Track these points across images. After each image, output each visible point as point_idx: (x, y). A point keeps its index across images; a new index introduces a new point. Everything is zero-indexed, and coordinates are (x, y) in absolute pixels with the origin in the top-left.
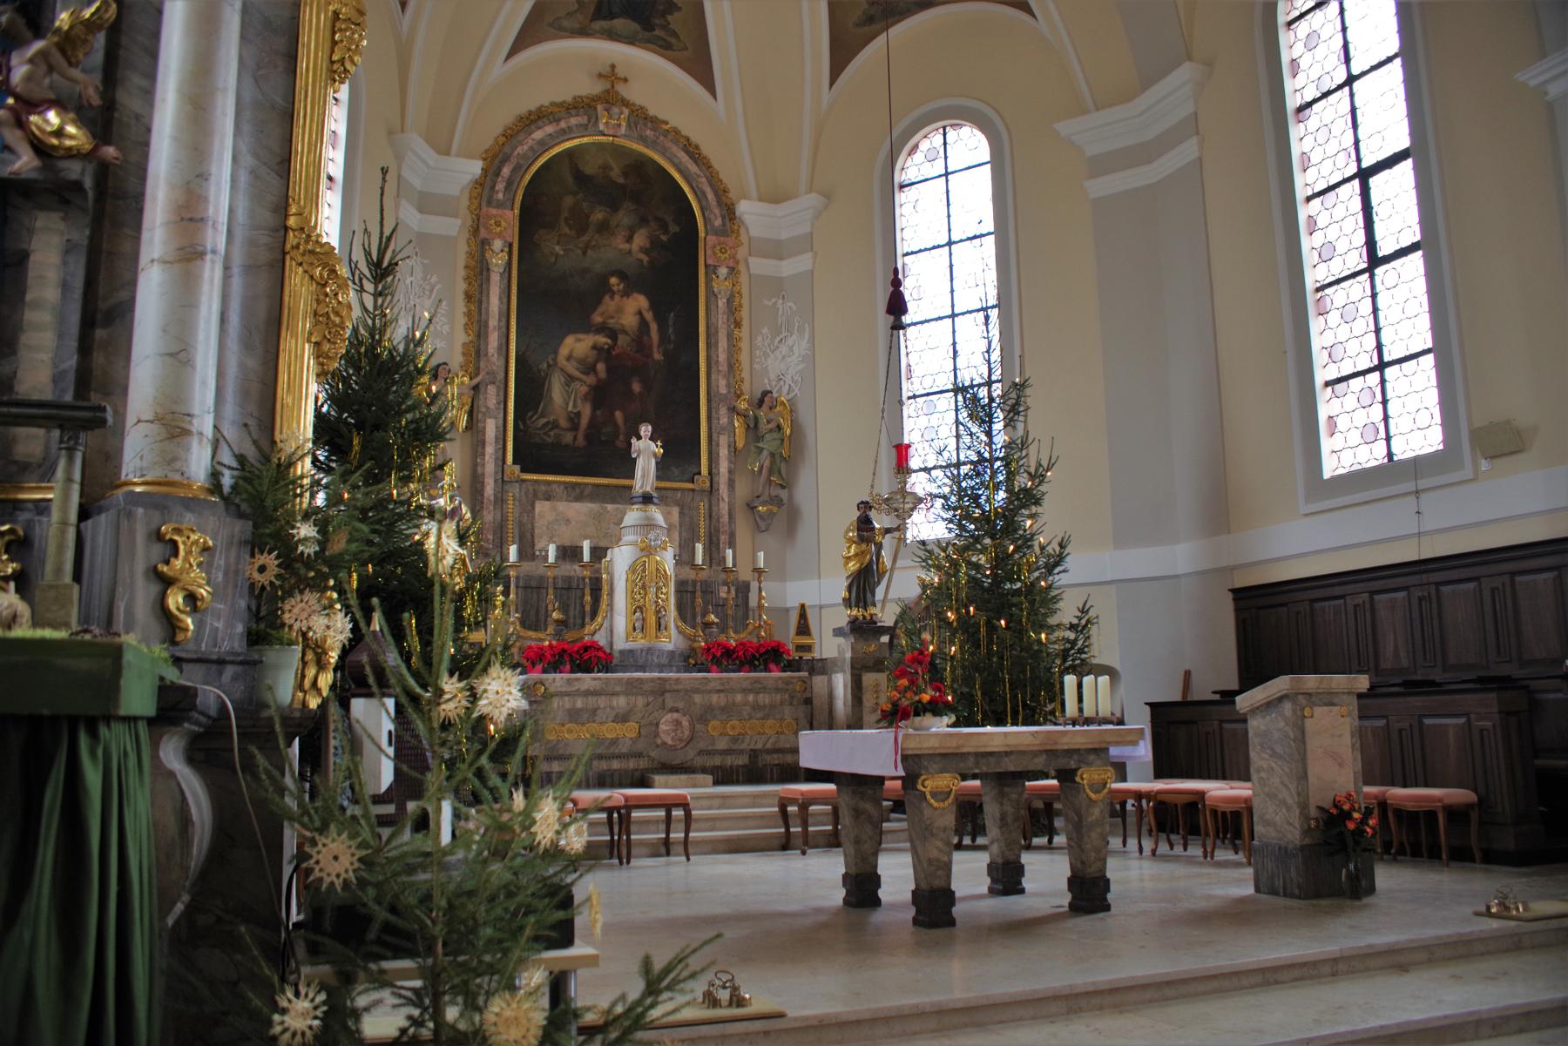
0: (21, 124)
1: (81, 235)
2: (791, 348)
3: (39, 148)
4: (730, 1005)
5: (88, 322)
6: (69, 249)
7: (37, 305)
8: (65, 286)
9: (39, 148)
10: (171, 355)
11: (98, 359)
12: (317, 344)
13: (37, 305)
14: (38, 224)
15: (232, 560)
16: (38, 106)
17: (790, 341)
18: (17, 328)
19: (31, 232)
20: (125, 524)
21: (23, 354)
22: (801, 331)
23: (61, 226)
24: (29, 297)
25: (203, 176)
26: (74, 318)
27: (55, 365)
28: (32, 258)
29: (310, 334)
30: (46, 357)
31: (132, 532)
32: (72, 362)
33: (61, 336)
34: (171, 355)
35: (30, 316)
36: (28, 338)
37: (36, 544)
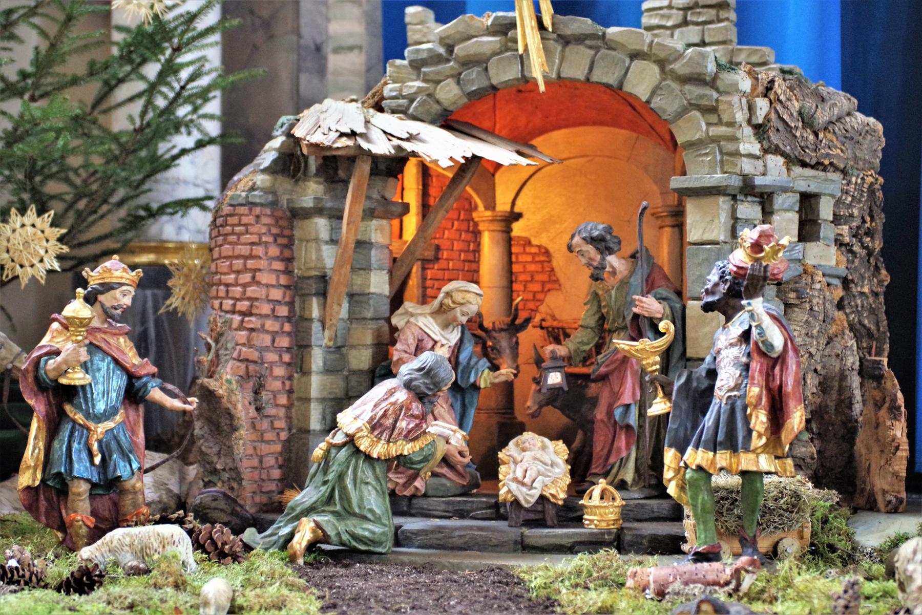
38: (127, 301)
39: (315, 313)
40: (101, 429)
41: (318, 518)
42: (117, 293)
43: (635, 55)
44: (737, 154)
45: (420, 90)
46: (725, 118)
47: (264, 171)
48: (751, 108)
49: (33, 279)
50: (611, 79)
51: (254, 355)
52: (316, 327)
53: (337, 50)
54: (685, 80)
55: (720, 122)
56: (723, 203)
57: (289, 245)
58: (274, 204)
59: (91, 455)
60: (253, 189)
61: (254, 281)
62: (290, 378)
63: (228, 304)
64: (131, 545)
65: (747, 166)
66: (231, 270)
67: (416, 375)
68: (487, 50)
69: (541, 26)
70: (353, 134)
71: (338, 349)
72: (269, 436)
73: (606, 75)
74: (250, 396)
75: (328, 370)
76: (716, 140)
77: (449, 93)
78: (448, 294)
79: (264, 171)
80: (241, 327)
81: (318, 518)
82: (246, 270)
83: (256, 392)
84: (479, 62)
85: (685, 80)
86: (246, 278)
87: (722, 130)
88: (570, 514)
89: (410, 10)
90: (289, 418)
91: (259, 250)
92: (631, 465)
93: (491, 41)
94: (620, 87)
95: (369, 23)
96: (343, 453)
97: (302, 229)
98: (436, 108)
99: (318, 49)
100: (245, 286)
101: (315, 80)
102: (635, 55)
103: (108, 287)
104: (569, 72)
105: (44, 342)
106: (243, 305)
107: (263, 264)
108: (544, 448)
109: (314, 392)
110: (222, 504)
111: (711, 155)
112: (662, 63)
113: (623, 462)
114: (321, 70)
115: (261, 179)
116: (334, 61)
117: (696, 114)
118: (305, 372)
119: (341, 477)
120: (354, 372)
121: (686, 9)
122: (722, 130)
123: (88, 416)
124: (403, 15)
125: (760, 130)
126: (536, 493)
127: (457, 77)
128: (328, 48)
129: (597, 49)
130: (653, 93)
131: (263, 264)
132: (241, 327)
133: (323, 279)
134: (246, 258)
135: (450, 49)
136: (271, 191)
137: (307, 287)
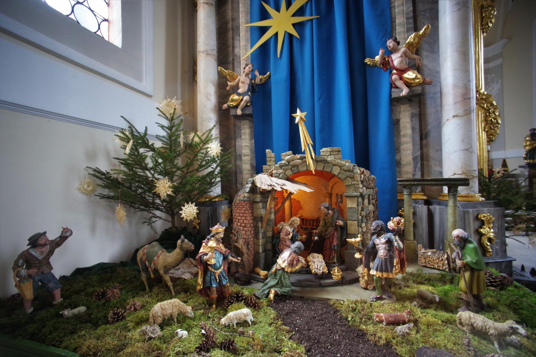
0: (401, 78)
1: (416, 111)
2: (493, 88)
3: (408, 84)
4: (454, 251)
5: (421, 139)
6: (413, 116)
7: (405, 136)
8: (413, 129)
9: (408, 84)
10: (467, 150)
11: (425, 150)
12: (487, 132)
13: (405, 136)
14: (402, 109)
15: (500, 224)
16: (404, 71)
17: (493, 86)
18: (400, 144)
19: (400, 112)
20: (467, 216)
21: (403, 152)
22: (497, 82)
23: (409, 108)
24: (402, 134)
25: (469, 81)
26: (418, 138)
27: (413, 155)
28: (401, 121)
29: (485, 128)
30: (410, 152)
31: (469, 218)
32: (419, 153)
33: (414, 145)
34: (467, 150)
35: (403, 140)
36: (403, 147)
37: (418, 214)
38: (222, 236)
39: (260, 225)
40: (218, 271)
41: (276, 289)
42: (220, 234)
43: (334, 165)
44: (359, 188)
45: (282, 173)
46: (356, 180)
47: (247, 193)
48: (361, 177)
49: (184, 206)
50: (329, 170)
51: (246, 237)
52: (260, 228)
53: (244, 156)
54: (346, 171)
55: (355, 181)
56: (356, 198)
57: (252, 210)
58: (249, 201)
59: (216, 280)
60: (244, 197)
61: (246, 219)
62: (254, 240)
63: (239, 224)
64: (236, 318)
65: (361, 190)
66: (239, 216)
67: (296, 249)
68: (299, 163)
69: (312, 158)
70: (271, 185)
71: (264, 233)
72: (251, 255)
73: (328, 170)
74: (246, 246)
75: (263, 238)
76: (354, 184)
77: (289, 173)
78: (293, 221)
79: (247, 193)
80: (243, 230)
81: (276, 289)
82: (243, 216)
83: (248, 246)
84: (296, 166)
85: (346, 171)
86: (244, 218)
87: (355, 182)
88: (328, 275)
89: (267, 150)
90: (254, 249)
91: (247, 212)
92: (336, 258)
93: (299, 161)
94: (331, 171)
95: (251, 150)
96: (280, 272)
97: (255, 206)
98: (286, 177)
99: (240, 155)
100: (243, 220)
101: (240, 162)
102: (334, 165)
103: (217, 233)
104: (318, 169)
105: (200, 252)
106: (243, 225)
107: (248, 215)
108: (318, 257)
109: (260, 244)
110: (243, 277)
111: (352, 189)
112: (340, 167)
113: (333, 258)
114: (241, 160)
115: (246, 195)
116: (243, 158)
117: (349, 178)
118: (258, 239)
119: (280, 278)
120: (268, 237)
121: (331, 152)
122: (355, 182)
123: (215, 269)
124: (265, 151)
125: (362, 182)
126: (321, 271)
127: (291, 170)
128: (242, 156)
129: (325, 164)
130: (339, 174)
131: (248, 215)
132: (243, 230)
133: (261, 217)
134: (243, 214)
135: (289, 163)
136: (249, 197)
137: (257, 219)
